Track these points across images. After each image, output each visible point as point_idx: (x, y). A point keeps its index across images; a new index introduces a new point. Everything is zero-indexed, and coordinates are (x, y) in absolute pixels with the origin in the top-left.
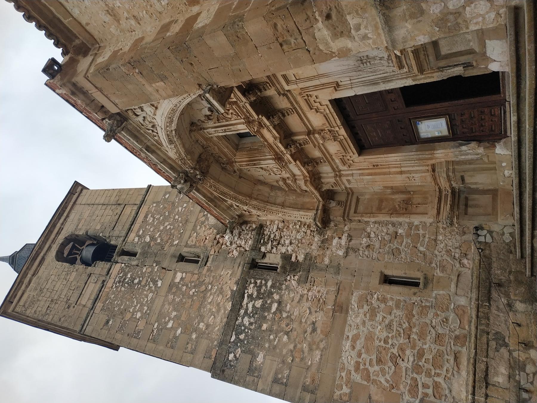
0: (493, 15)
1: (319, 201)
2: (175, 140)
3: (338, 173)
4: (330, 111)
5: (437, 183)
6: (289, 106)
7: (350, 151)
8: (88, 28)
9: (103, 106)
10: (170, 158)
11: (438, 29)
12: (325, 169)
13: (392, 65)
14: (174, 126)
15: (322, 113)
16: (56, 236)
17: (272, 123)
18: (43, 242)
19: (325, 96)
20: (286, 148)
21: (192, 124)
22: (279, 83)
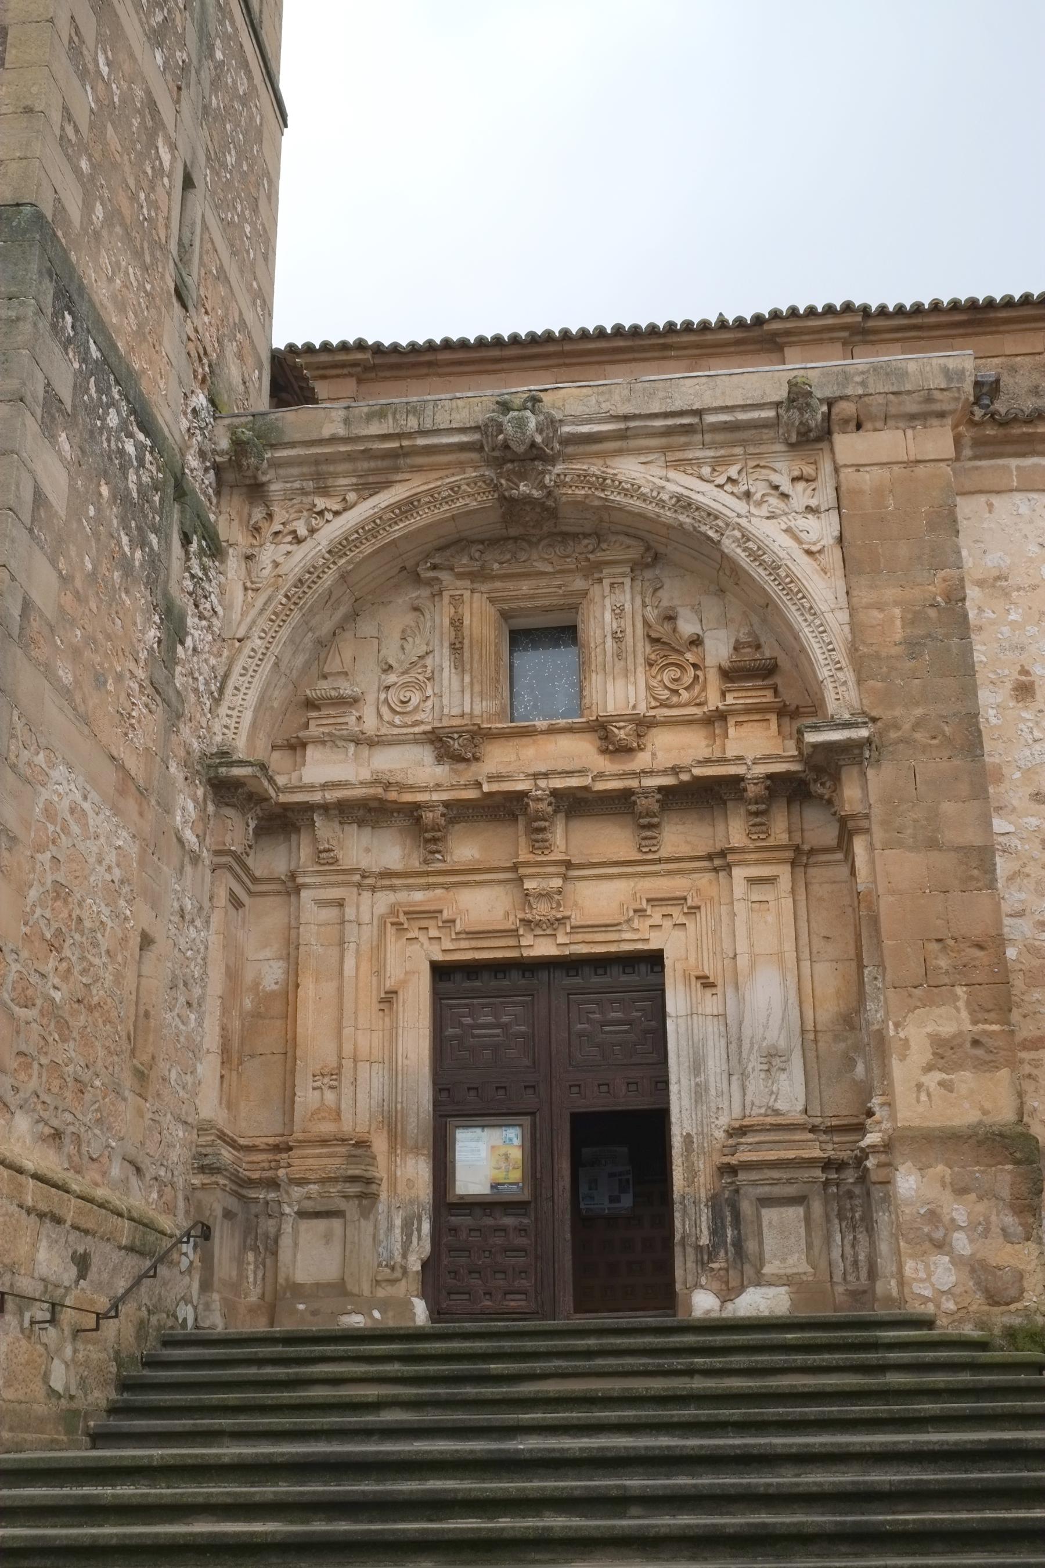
2: (683, 518)
5: (304, 1143)
7: (464, 944)
8: (982, 499)
9: (859, 427)
10: (620, 452)
11: (922, 1211)
13: (753, 1113)
14: (729, 546)
15: (629, 921)
17: (646, 792)
20: (555, 793)
21: (656, 557)
22: (757, 862)
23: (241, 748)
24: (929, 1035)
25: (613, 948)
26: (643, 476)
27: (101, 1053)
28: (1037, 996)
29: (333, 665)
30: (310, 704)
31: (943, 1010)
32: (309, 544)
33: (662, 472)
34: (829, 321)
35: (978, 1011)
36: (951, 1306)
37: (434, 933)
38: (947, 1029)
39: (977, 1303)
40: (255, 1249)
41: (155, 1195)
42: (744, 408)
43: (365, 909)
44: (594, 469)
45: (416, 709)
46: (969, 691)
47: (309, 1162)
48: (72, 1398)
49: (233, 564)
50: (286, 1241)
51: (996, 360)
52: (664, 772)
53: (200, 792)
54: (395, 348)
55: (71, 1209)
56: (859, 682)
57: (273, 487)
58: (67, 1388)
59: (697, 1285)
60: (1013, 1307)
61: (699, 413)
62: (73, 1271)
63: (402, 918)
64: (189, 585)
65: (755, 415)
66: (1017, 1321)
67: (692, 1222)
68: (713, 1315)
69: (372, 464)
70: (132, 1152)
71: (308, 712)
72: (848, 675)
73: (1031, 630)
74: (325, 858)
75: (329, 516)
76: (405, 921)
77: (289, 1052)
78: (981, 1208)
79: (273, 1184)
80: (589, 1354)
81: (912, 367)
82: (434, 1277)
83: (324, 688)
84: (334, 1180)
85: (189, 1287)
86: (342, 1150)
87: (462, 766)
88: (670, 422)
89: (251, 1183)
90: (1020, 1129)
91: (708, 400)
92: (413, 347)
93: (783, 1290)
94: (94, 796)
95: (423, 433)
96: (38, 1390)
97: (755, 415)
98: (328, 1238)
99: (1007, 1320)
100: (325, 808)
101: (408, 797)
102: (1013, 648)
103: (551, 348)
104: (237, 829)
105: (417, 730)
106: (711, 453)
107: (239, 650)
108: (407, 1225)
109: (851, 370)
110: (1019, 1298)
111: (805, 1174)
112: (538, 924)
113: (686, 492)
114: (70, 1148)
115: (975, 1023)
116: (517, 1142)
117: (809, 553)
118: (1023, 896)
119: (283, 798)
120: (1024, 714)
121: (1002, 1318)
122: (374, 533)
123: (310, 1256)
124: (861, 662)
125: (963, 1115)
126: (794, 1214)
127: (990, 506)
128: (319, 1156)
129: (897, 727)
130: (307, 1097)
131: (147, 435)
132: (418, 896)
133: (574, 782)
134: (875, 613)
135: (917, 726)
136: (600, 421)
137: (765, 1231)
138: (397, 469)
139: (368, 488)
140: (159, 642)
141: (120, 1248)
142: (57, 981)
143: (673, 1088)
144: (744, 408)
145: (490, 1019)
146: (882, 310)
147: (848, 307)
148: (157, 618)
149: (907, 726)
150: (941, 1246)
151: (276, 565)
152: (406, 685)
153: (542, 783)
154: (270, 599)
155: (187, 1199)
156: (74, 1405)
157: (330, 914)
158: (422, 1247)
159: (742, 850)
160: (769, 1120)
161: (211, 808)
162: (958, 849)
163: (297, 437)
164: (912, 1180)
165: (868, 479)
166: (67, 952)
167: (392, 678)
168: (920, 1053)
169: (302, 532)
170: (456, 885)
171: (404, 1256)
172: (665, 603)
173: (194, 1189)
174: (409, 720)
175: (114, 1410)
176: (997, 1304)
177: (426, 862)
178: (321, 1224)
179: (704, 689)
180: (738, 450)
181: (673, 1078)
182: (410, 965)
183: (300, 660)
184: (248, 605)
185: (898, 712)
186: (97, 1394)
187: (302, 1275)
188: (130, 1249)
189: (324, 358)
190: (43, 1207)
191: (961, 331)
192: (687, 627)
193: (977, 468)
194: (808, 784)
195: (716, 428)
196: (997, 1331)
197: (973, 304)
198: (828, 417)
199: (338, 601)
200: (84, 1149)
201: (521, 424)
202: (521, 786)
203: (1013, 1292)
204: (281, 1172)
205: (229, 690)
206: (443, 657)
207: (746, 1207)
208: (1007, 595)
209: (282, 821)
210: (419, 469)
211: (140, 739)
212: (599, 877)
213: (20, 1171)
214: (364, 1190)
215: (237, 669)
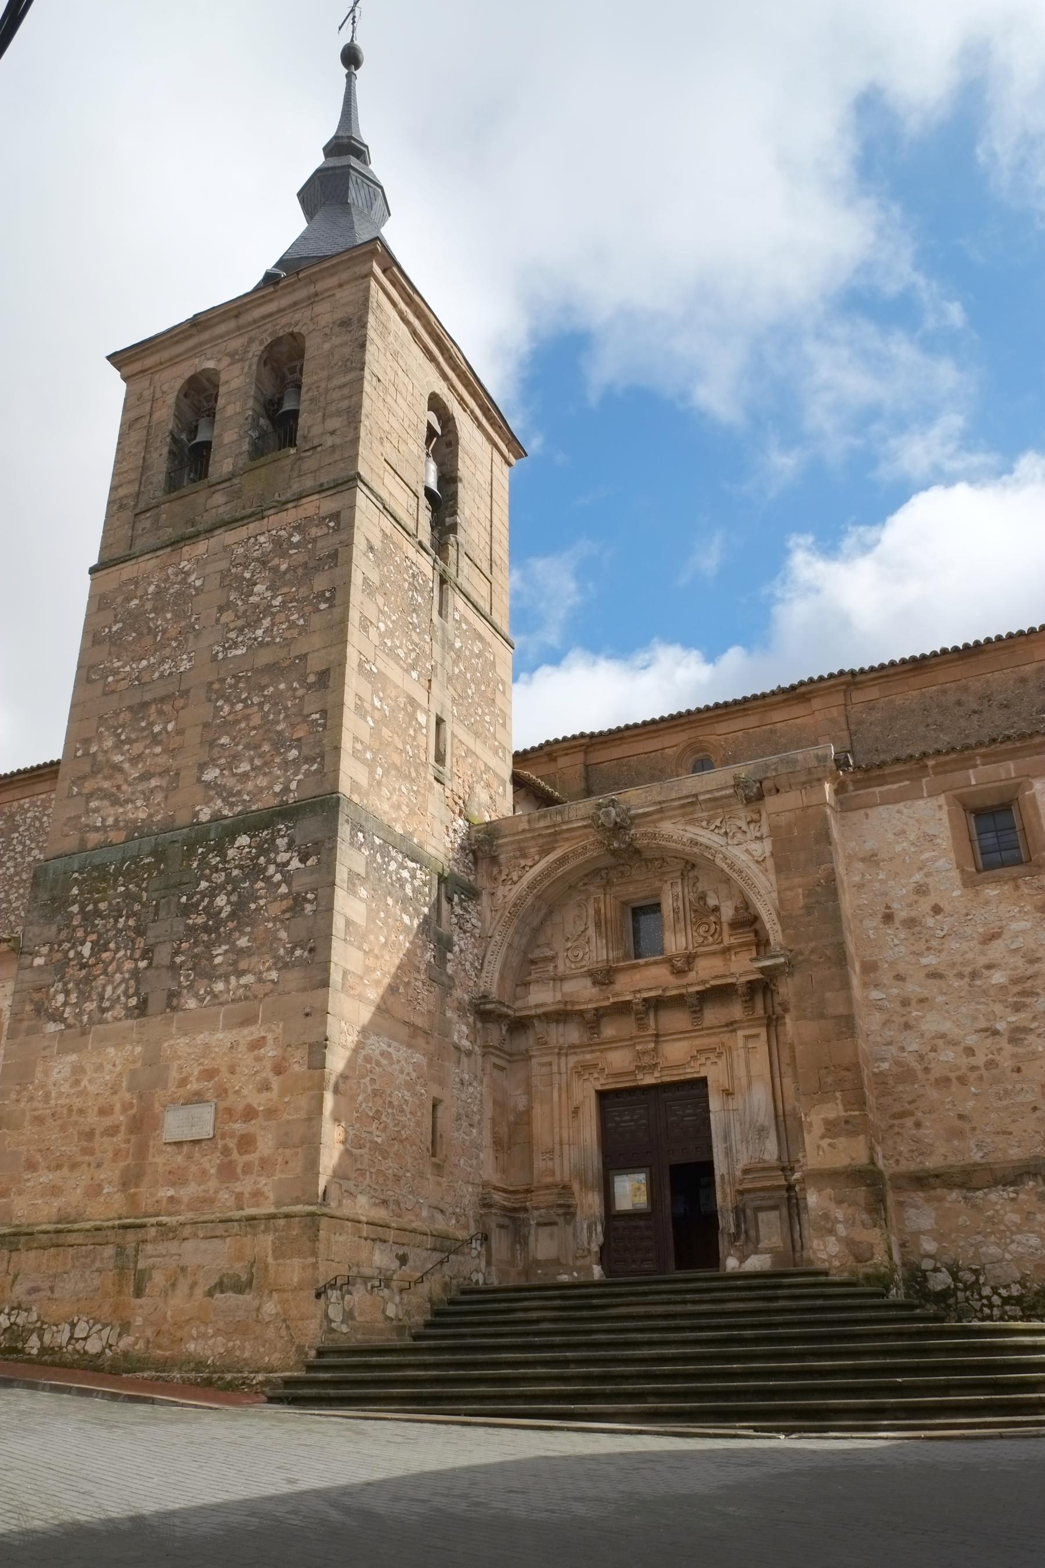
0: (825, 1257)
1: (515, 1010)
3: (564, 1051)
4: (691, 1073)
6: (706, 1023)
7: (610, 1080)
8: (862, 811)
10: (661, 819)
12: (573, 1034)
14: (719, 862)
15: (689, 1063)
16: (459, 395)
17: (690, 994)
18: (458, 366)
19: (714, 1074)
20: (645, 1000)
21: (694, 866)
22: (749, 1027)
23: (494, 992)
24: (823, 1119)
25: (682, 1078)
26: (675, 831)
27: (409, 1160)
28: (900, 1088)
29: (542, 940)
30: (533, 962)
31: (829, 1105)
32: (519, 884)
33: (681, 827)
34: (832, 682)
35: (847, 1105)
36: (837, 1263)
37: (596, 1075)
38: (832, 1115)
39: (851, 1261)
40: (520, 1243)
41: (454, 1221)
42: (717, 790)
43: (563, 1065)
44: (649, 830)
45: (582, 959)
46: (838, 931)
47: (542, 1198)
48: (400, 1320)
49: (485, 898)
50: (532, 1239)
51: (934, 688)
52: (698, 984)
53: (471, 1020)
54: (601, 733)
55: (391, 1235)
56: (783, 931)
57: (501, 857)
58: (397, 1315)
59: (729, 1254)
60: (868, 1263)
61: (696, 796)
62: (398, 1263)
63: (580, 1069)
64: (454, 920)
65: (723, 793)
66: (870, 1270)
67: (727, 1222)
68: (736, 1270)
69: (545, 840)
70: (435, 1203)
71: (527, 966)
72: (778, 927)
73: (891, 883)
74: (542, 1042)
75: (527, 869)
76: (584, 1069)
77: (529, 1143)
78: (850, 1211)
79: (525, 1210)
80: (645, 1294)
81: (800, 757)
82: (605, 1256)
83: (537, 954)
84: (552, 1206)
85: (479, 1264)
86: (556, 1191)
87: (604, 987)
88: (682, 802)
89: (515, 1210)
90: (871, 1167)
91: (698, 789)
92: (610, 732)
93: (768, 1256)
94: (395, 1044)
95: (564, 823)
96: (380, 1316)
97: (723, 793)
98: (552, 1236)
99: (865, 1270)
100: (538, 1017)
101: (577, 1008)
102: (881, 894)
103: (683, 720)
104: (496, 1033)
105: (583, 970)
106: (706, 814)
107: (489, 943)
108: (589, 1228)
109: (769, 762)
110: (871, 1259)
111: (777, 1194)
112: (645, 1067)
113: (694, 837)
114: (392, 1206)
115: (846, 1111)
116: (644, 1181)
117: (757, 862)
118: (892, 1033)
119: (517, 1014)
120: (889, 931)
121: (864, 1269)
122: (548, 875)
123: (544, 1246)
124: (784, 919)
125: (841, 1161)
126: (773, 1215)
127: (867, 815)
128: (545, 1195)
129: (801, 953)
130: (539, 1164)
131: (417, 862)
132: (588, 1056)
133: (653, 994)
134: (789, 893)
135: (812, 952)
136: (648, 806)
137: (760, 1224)
138: (557, 841)
139: (544, 852)
140: (434, 957)
141: (427, 1249)
142: (378, 1133)
143: (715, 1150)
144: (717, 790)
145: (628, 1118)
146: (862, 671)
147: (841, 673)
148: (432, 946)
149: (807, 953)
150: (831, 1231)
151: (505, 897)
152: (577, 947)
153: (638, 996)
154: (502, 915)
155: (476, 1221)
156: (401, 1323)
157: (545, 1070)
158: (599, 1238)
159: (741, 1021)
160: (760, 1165)
161: (479, 1025)
162: (835, 1017)
163: (507, 832)
164: (814, 1197)
165: (783, 820)
166: (384, 1118)
167: (569, 944)
168: (818, 1129)
169: (515, 878)
170: (605, 1049)
171: (589, 1244)
172: (700, 890)
173: (481, 1215)
174: (579, 965)
175: (428, 1325)
176: (860, 1262)
177: (591, 1039)
178: (548, 1229)
179: (721, 934)
180: (720, 810)
181: (714, 1144)
182: (585, 1093)
183: (524, 940)
184: (493, 919)
185: (802, 946)
186: (417, 1318)
187: (540, 1256)
188: (434, 1249)
189: (565, 744)
190: (372, 1236)
191: (912, 674)
192: (712, 901)
193: (858, 795)
194: (761, 987)
195: (705, 801)
196: (860, 1276)
197: (913, 659)
198: (760, 789)
199: (539, 909)
200: (402, 1205)
201: (607, 814)
202: (628, 998)
203: (868, 1255)
204: (528, 1204)
205: (486, 964)
206: (591, 931)
207: (749, 1213)
208: (878, 864)
209: (519, 1025)
210: (567, 840)
211: (424, 1008)
212: (674, 1040)
213: (359, 1222)
214: (568, 1212)
215: (489, 953)
